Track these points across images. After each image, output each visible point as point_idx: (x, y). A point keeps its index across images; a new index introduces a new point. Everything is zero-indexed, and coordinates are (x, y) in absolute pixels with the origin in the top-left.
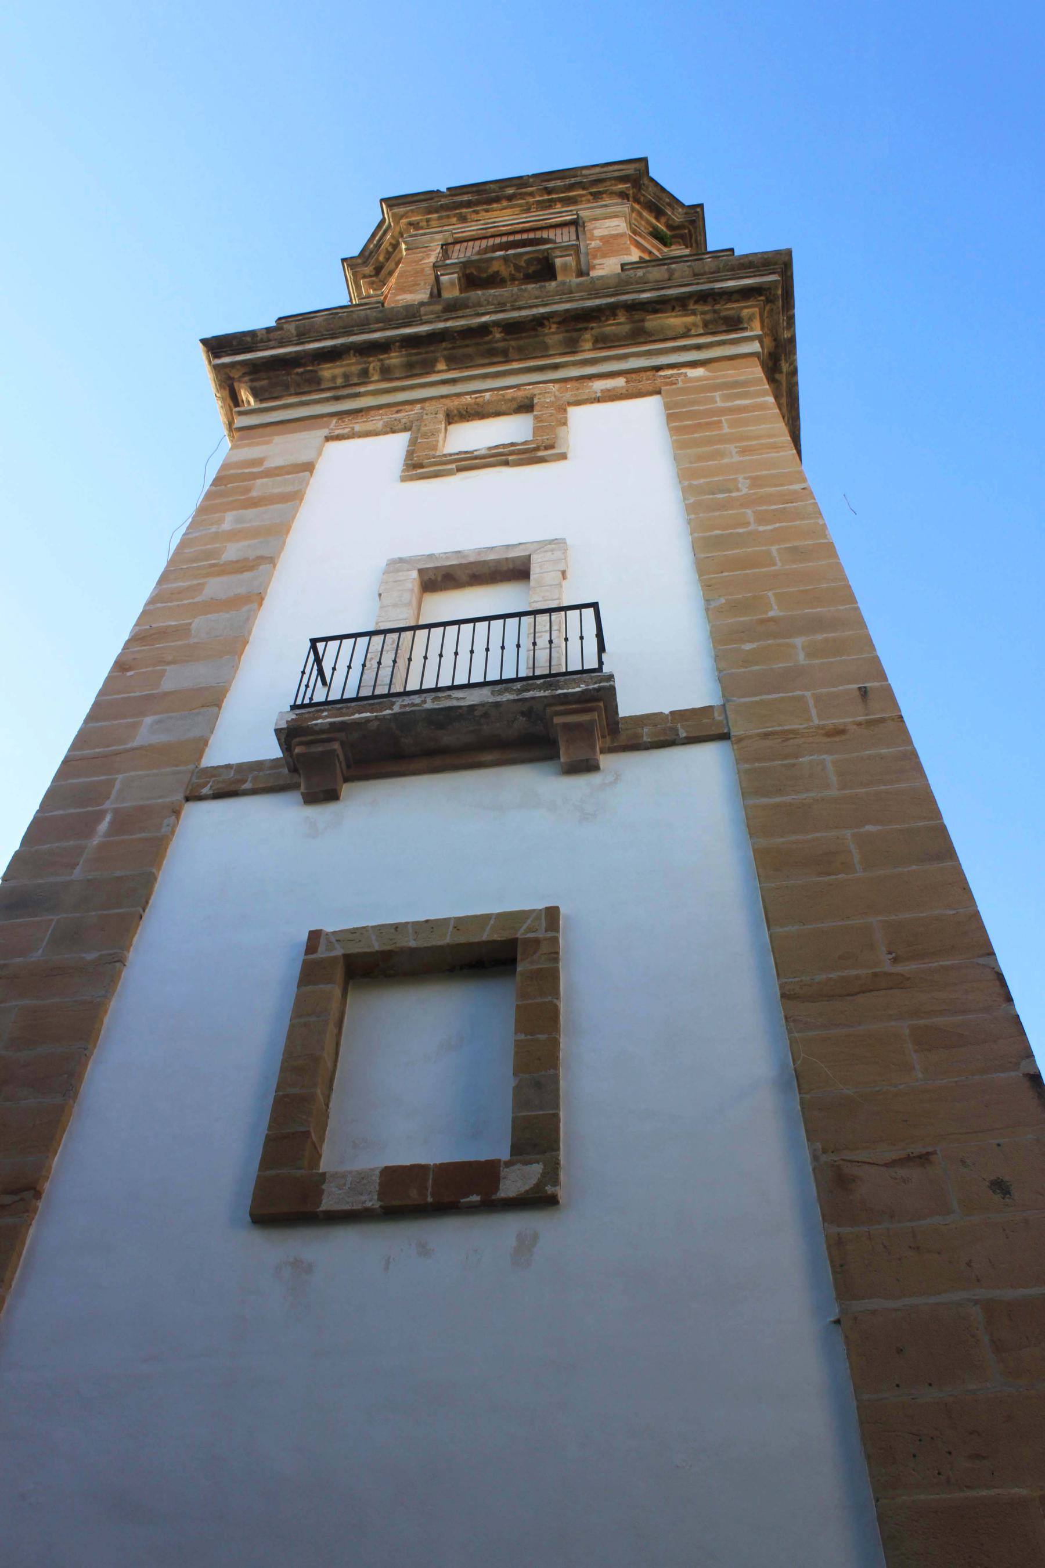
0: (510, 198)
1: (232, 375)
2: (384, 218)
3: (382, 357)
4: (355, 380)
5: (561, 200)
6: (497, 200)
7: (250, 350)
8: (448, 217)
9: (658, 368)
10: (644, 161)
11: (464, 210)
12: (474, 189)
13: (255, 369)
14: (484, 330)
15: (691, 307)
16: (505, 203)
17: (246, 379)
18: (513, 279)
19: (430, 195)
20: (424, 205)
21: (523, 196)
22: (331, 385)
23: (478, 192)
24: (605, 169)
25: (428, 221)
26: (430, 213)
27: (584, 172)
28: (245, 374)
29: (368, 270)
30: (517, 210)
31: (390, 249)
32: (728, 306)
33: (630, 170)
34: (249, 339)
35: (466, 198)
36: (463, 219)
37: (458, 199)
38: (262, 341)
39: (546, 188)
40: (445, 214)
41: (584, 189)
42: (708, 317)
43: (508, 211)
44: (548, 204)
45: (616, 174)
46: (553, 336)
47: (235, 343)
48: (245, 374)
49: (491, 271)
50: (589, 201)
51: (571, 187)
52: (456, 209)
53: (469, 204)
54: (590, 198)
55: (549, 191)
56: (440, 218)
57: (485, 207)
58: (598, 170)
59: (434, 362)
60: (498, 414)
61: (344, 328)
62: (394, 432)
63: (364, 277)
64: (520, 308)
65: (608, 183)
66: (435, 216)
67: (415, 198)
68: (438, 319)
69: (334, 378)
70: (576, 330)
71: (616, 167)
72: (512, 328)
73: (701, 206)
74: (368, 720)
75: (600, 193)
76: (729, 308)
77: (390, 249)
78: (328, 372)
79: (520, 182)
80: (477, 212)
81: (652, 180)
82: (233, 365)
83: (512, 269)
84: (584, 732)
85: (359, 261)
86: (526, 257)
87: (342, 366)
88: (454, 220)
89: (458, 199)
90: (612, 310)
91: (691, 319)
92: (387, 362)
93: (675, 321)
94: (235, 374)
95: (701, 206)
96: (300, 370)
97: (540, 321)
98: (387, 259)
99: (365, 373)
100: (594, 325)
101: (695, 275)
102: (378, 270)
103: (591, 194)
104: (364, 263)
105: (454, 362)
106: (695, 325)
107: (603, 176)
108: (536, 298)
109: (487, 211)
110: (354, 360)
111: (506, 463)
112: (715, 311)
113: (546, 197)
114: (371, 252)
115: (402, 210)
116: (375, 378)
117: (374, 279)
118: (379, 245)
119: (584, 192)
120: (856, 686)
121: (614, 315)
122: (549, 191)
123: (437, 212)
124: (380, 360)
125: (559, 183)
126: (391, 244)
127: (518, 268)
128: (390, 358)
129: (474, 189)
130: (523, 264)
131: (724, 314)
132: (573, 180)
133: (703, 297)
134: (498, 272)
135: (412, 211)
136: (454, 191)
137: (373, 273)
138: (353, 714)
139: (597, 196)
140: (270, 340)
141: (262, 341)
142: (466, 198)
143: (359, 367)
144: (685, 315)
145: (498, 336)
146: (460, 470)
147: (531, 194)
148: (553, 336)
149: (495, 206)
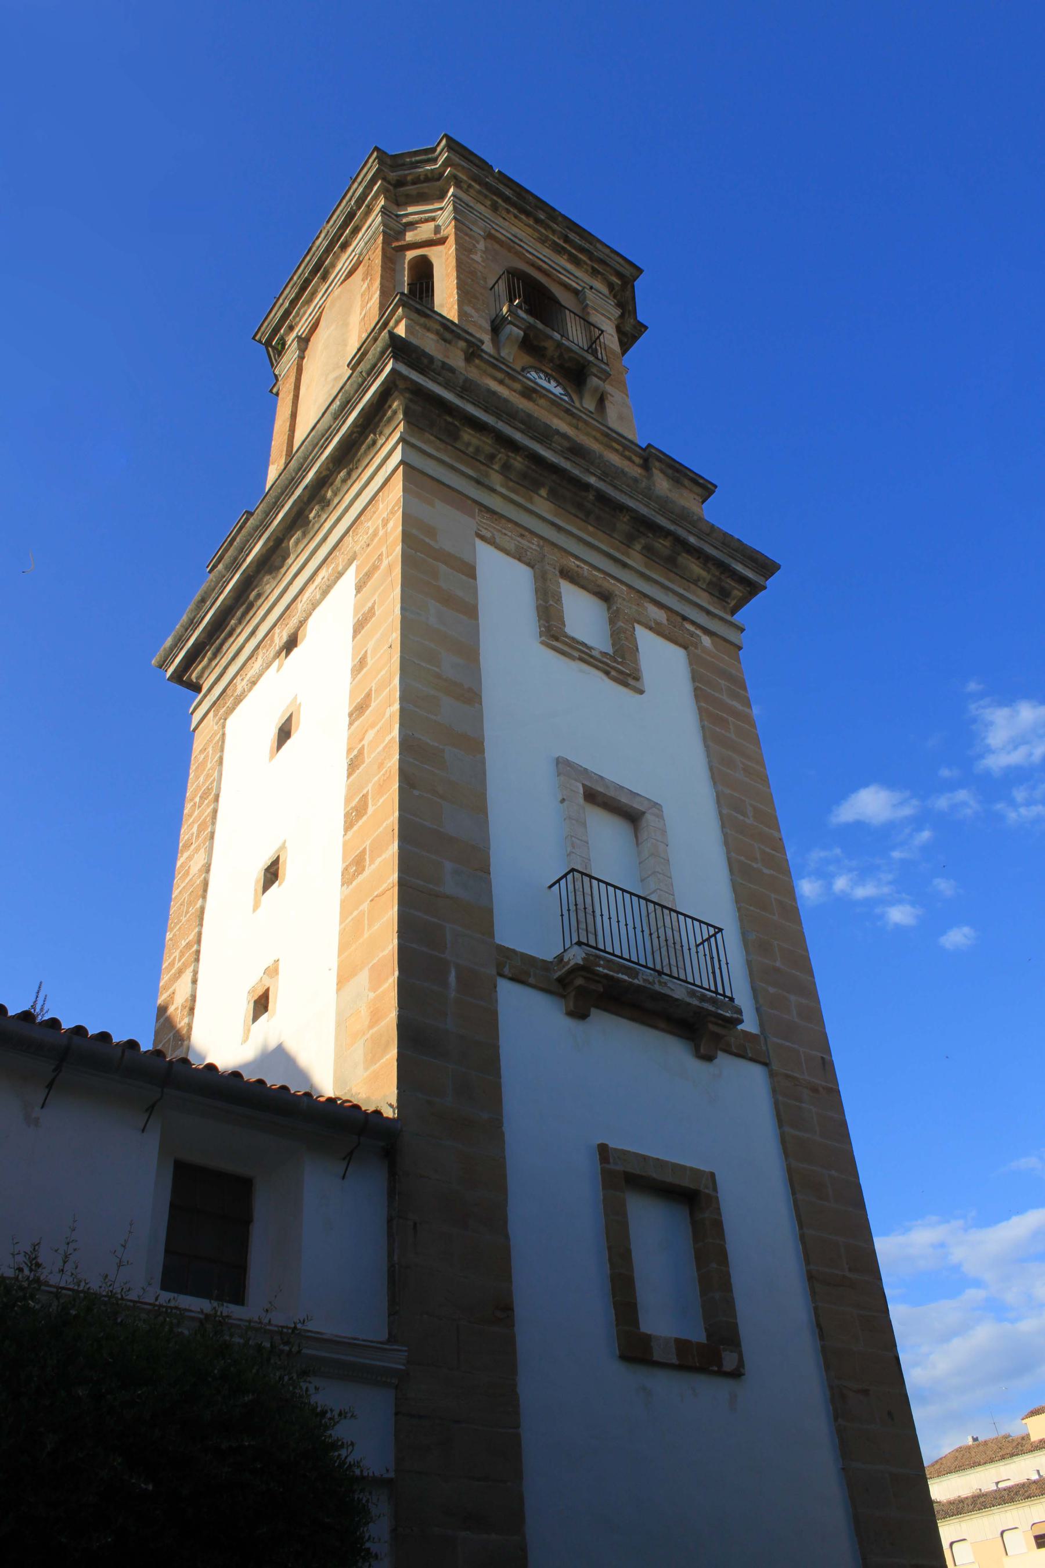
0: (537, 221)
1: (398, 382)
2: (434, 150)
3: (510, 454)
4: (482, 458)
5: (570, 254)
6: (528, 214)
7: (422, 372)
8: (486, 196)
9: (685, 618)
10: (640, 271)
11: (500, 201)
12: (518, 190)
13: (418, 393)
14: (587, 487)
15: (710, 565)
16: (531, 222)
17: (407, 395)
18: (551, 360)
19: (484, 165)
20: (475, 170)
21: (547, 227)
22: (463, 448)
23: (519, 195)
24: (612, 255)
25: (470, 186)
26: (475, 180)
27: (598, 245)
28: (407, 389)
29: (393, 176)
30: (536, 235)
31: (422, 178)
32: (729, 581)
33: (627, 271)
34: (426, 361)
35: (508, 192)
36: (495, 208)
37: (501, 187)
38: (434, 371)
39: (566, 236)
40: (485, 191)
41: (590, 259)
42: (714, 579)
43: (529, 231)
44: (558, 250)
45: (618, 267)
46: (623, 524)
47: (414, 356)
48: (407, 389)
49: (543, 344)
50: (586, 272)
51: (582, 250)
52: (495, 194)
53: (507, 199)
54: (590, 270)
55: (566, 239)
56: (479, 192)
57: (516, 212)
58: (607, 251)
59: (543, 485)
60: (583, 587)
61: (497, 408)
62: (519, 560)
63: (384, 179)
64: (615, 487)
65: (608, 269)
66: (477, 187)
67: (472, 158)
68: (561, 453)
69: (468, 444)
70: (638, 531)
71: (620, 260)
72: (602, 498)
73: (646, 328)
74: (625, 981)
75: (599, 272)
76: (729, 583)
77: (422, 178)
78: (468, 435)
79: (553, 214)
80: (508, 211)
81: (633, 286)
82: (406, 378)
83: (557, 354)
84: (717, 1038)
85: (389, 161)
86: (572, 355)
87: (480, 440)
88: (488, 203)
89: (501, 187)
90: (668, 534)
91: (704, 574)
92: (512, 461)
93: (696, 568)
94: (401, 385)
95: (646, 328)
96: (450, 419)
97: (622, 508)
98: (414, 183)
99: (492, 457)
100: (650, 535)
101: (723, 543)
102: (400, 183)
103: (593, 268)
104: (391, 166)
105: (554, 496)
106: (704, 579)
107: (608, 260)
108: (628, 486)
109: (516, 217)
110: (489, 441)
111: (607, 673)
112: (720, 579)
113: (561, 242)
114: (403, 165)
115: (456, 159)
116: (496, 467)
117: (391, 188)
118: (415, 165)
119: (589, 262)
120: (820, 1054)
121: (666, 537)
122: (566, 239)
123: (480, 184)
124: (508, 456)
125: (577, 239)
126: (426, 175)
127: (561, 356)
128: (515, 459)
129: (518, 190)
130: (566, 357)
131: (723, 584)
132: (587, 246)
133: (721, 565)
134: (545, 348)
135: (463, 167)
136: (503, 177)
137: (393, 182)
138: (618, 973)
139: (595, 273)
140: (439, 375)
141: (434, 371)
142: (508, 192)
143: (493, 451)
144: (704, 569)
145: (591, 497)
146: (581, 659)
147: (554, 232)
148: (623, 524)
149: (523, 217)
